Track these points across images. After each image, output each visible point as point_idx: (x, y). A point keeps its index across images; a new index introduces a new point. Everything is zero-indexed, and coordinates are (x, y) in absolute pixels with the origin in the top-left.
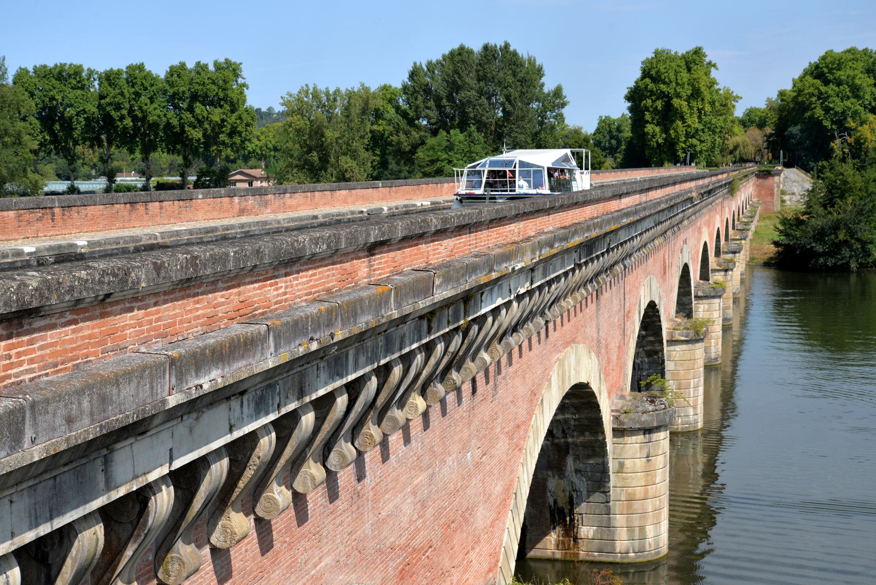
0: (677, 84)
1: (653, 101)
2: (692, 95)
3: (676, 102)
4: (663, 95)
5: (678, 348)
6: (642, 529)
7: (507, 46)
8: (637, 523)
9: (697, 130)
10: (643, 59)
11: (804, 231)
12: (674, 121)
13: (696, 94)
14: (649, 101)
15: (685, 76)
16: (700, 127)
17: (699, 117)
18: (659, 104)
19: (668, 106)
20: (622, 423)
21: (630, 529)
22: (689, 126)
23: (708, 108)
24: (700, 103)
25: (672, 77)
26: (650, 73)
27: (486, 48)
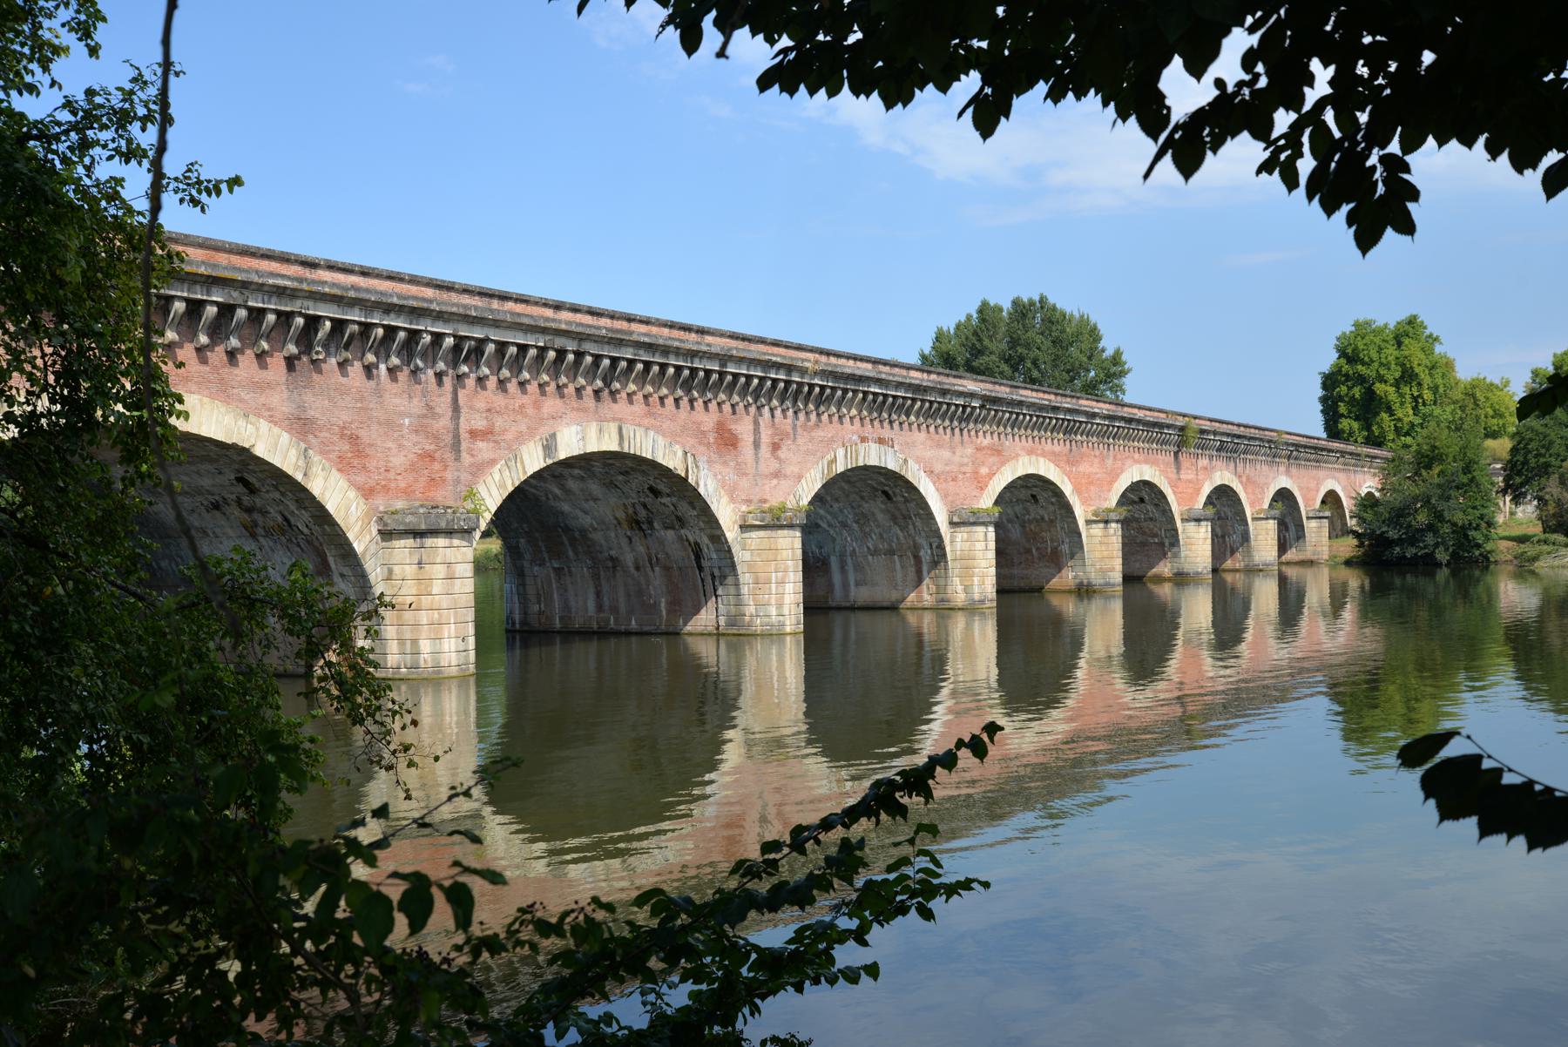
0: (1381, 364)
1: (1350, 388)
2: (1402, 377)
3: (1379, 388)
4: (1361, 380)
5: (755, 534)
6: (415, 642)
7: (1043, 300)
8: (408, 636)
9: (1412, 425)
10: (1339, 334)
11: (1376, 514)
12: (1377, 414)
13: (1408, 376)
14: (1344, 388)
15: (1391, 352)
16: (1417, 421)
17: (1415, 408)
18: (1357, 392)
19: (1370, 394)
20: (386, 525)
21: (401, 641)
22: (1400, 420)
23: (1428, 395)
24: (1415, 389)
25: (1375, 356)
26: (1349, 353)
27: (1016, 303)
